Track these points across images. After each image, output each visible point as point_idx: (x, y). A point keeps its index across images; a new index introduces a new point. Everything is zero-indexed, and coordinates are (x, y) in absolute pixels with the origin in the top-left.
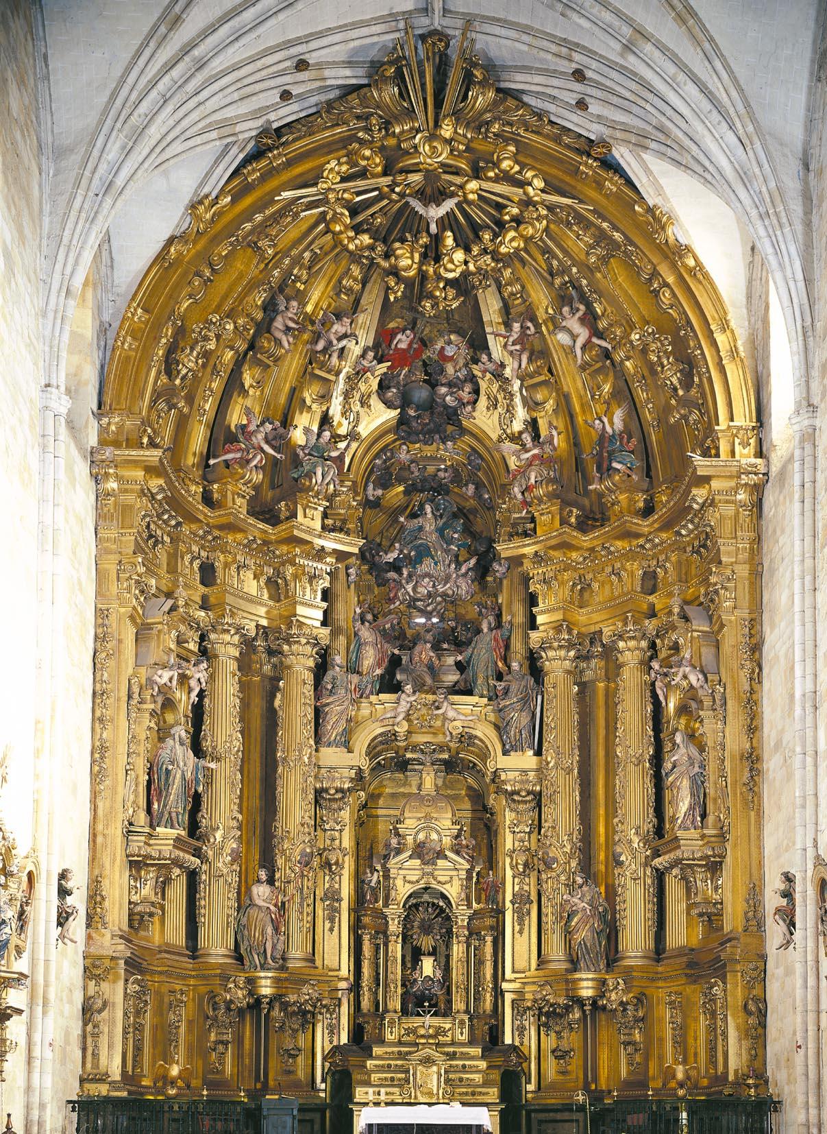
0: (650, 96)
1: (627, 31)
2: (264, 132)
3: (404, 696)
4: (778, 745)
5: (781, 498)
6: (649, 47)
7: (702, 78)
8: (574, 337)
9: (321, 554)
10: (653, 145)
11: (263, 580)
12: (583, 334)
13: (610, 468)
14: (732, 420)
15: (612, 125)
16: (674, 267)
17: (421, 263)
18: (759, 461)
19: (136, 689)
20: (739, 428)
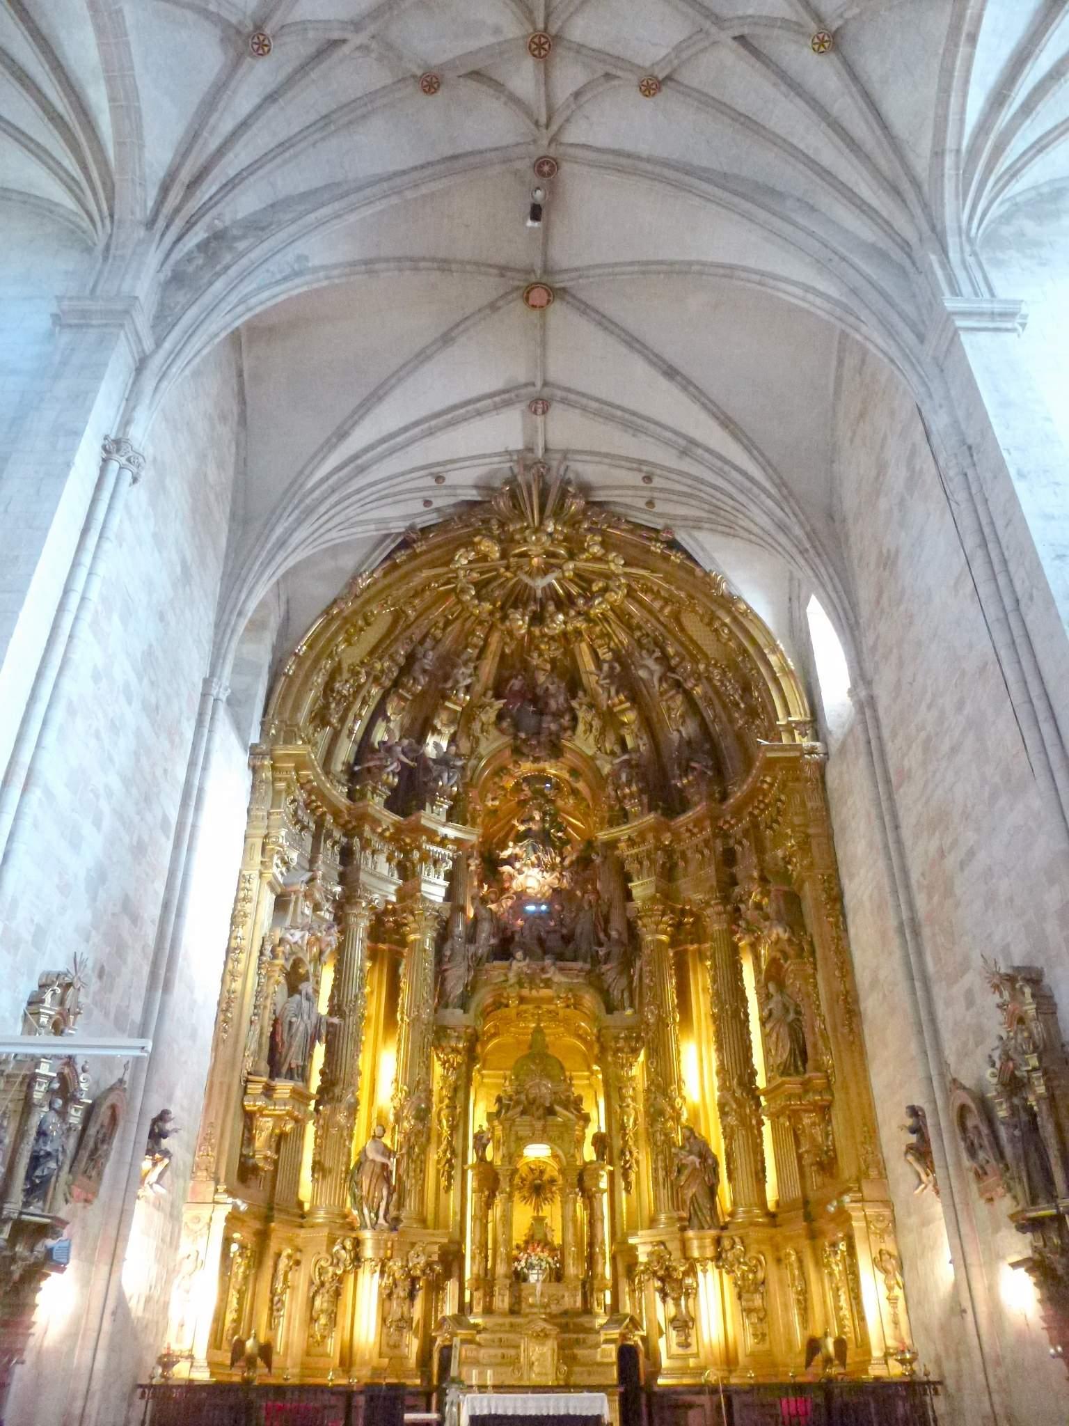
0: (703, 487)
1: (683, 442)
2: (411, 528)
4: (875, 982)
5: (845, 767)
6: (700, 451)
8: (651, 673)
9: (443, 842)
10: (707, 525)
11: (394, 863)
12: (656, 668)
13: (688, 766)
14: (789, 714)
15: (674, 517)
16: (729, 612)
17: (530, 625)
19: (268, 948)
20: (798, 723)
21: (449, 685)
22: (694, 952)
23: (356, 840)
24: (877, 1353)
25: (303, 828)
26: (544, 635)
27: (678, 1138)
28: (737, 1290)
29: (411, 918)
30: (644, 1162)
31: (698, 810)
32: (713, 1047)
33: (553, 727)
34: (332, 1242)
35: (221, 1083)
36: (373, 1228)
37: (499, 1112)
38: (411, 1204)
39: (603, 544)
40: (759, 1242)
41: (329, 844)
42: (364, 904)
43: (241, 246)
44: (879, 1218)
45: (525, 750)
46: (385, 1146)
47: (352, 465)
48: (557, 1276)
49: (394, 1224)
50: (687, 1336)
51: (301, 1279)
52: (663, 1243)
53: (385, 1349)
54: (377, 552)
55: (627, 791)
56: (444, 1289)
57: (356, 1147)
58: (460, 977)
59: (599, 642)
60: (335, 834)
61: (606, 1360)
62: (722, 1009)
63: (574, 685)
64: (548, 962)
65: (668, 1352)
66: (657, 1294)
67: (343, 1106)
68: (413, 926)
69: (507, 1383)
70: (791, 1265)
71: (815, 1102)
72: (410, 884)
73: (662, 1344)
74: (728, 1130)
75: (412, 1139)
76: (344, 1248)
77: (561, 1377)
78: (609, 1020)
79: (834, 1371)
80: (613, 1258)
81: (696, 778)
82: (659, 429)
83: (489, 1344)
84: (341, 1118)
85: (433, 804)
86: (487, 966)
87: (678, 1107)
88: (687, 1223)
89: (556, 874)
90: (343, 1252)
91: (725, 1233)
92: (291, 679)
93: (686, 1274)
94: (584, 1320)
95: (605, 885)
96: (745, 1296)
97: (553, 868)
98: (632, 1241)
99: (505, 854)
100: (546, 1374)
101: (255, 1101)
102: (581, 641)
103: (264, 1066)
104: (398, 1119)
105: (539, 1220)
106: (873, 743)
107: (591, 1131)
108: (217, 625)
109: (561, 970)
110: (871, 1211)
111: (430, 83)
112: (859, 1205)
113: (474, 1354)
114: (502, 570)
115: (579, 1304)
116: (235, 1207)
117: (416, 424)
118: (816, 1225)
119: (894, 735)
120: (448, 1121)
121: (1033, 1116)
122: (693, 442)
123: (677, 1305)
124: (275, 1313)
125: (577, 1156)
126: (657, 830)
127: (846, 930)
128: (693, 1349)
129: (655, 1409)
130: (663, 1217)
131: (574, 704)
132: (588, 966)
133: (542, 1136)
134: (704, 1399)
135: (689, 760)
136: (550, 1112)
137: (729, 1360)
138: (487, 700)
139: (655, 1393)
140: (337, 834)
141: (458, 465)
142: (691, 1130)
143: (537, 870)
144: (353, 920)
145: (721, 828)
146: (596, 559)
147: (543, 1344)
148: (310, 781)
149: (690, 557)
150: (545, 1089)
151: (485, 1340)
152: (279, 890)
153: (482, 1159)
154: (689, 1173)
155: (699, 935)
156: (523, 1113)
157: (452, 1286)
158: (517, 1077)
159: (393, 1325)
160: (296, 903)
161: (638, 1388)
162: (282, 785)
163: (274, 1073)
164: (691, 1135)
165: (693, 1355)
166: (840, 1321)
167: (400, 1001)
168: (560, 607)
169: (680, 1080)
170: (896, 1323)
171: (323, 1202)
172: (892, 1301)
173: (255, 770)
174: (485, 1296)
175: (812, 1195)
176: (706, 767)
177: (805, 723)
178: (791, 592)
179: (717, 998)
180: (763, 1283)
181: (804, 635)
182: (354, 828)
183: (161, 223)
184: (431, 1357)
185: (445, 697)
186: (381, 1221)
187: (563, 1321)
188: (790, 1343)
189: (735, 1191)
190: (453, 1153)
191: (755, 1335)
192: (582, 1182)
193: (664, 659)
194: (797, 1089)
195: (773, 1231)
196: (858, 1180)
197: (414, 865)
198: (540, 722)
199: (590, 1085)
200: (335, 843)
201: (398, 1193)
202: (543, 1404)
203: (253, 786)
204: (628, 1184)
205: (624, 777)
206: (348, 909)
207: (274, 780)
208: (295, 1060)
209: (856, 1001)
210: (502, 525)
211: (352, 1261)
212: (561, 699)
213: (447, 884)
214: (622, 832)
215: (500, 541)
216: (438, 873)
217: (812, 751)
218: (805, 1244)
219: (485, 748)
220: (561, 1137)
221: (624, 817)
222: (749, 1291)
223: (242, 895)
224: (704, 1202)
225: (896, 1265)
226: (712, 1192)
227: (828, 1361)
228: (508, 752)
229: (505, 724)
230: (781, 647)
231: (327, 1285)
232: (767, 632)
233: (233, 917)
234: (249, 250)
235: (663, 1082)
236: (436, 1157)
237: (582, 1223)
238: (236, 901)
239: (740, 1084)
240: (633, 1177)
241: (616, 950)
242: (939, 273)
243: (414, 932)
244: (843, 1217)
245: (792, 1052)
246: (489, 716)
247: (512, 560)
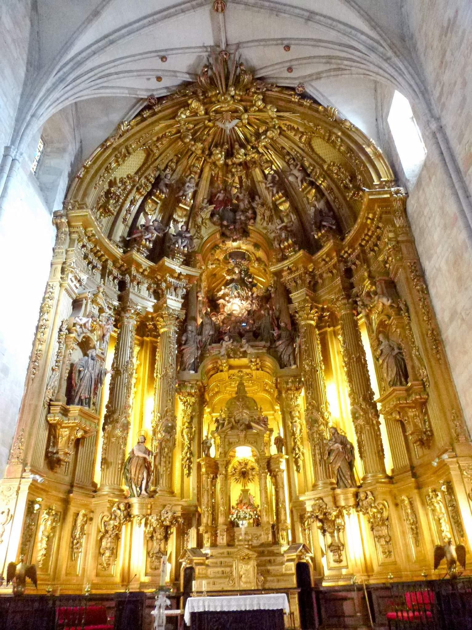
2: (152, 96)
3: (224, 343)
4: (454, 315)
11: (151, 291)
15: (305, 77)
16: (340, 129)
17: (225, 159)
19: (65, 326)
21: (181, 194)
22: (330, 332)
23: (127, 276)
25: (94, 267)
26: (233, 164)
27: (327, 435)
28: (370, 525)
29: (161, 319)
30: (306, 453)
31: (328, 246)
32: (345, 378)
33: (243, 218)
35: (30, 405)
38: (163, 482)
39: (264, 100)
40: (384, 493)
41: (111, 278)
42: (133, 311)
45: (228, 233)
46: (146, 449)
47: (107, 40)
48: (257, 523)
49: (152, 495)
51: (93, 529)
52: (321, 498)
53: (149, 570)
54: (132, 111)
55: (286, 244)
56: (187, 534)
57: (128, 450)
58: (191, 353)
59: (266, 165)
61: (288, 572)
62: (350, 359)
63: (253, 193)
65: (328, 566)
66: (319, 531)
67: (119, 425)
68: (163, 324)
69: (225, 589)
70: (405, 506)
71: (416, 399)
73: (323, 561)
74: (359, 428)
75: (163, 444)
76: (119, 509)
77: (260, 584)
79: (457, 569)
80: (292, 512)
81: (326, 231)
82: (292, 9)
83: (215, 565)
84: (118, 432)
87: (326, 417)
88: (336, 486)
89: (249, 302)
90: (118, 511)
91: (361, 490)
93: (337, 517)
94: (274, 548)
95: (278, 304)
96: (376, 528)
97: (247, 298)
98: (301, 499)
99: (221, 293)
100: (250, 582)
101: (54, 416)
102: (255, 167)
104: (154, 433)
105: (245, 492)
106: (445, 154)
107: (275, 435)
108: (17, 120)
109: (252, 346)
112: (455, 459)
113: (204, 572)
114: (206, 122)
115: (270, 538)
117: (145, 18)
118: (421, 479)
119: (461, 137)
120: (188, 435)
122: (312, 12)
124: (75, 550)
125: (266, 451)
127: (428, 293)
128: (344, 564)
129: (322, 602)
130: (320, 483)
131: (254, 205)
132: (268, 344)
133: (246, 441)
134: (354, 595)
135: (321, 221)
136: (249, 427)
137: (368, 570)
138: (204, 205)
139: (321, 592)
140: (115, 272)
141: (174, 52)
142: (335, 429)
143: (238, 299)
145: (342, 257)
146: (260, 110)
147: (247, 564)
148: (93, 235)
149: (316, 102)
150: (245, 415)
151: (213, 563)
152: (74, 297)
154: (335, 456)
155: (333, 320)
156: (232, 428)
158: (228, 409)
159: (156, 557)
160: (86, 305)
161: (312, 589)
163: (70, 400)
164: (335, 431)
165: (343, 567)
167: (156, 366)
168: (242, 146)
169: (326, 402)
171: (108, 482)
173: (58, 227)
174: (212, 535)
175: (416, 462)
176: (332, 224)
177: (391, 182)
178: (377, 116)
179: (348, 353)
180: (387, 519)
181: (386, 131)
182: (126, 270)
184: (179, 575)
185: (179, 201)
186: (143, 492)
187: (261, 549)
188: (408, 557)
191: (384, 553)
192: (269, 466)
193: (304, 169)
194: (404, 394)
195: (392, 486)
197: (163, 291)
198: (235, 216)
199: (275, 419)
200: (115, 278)
202: (242, 603)
203: (57, 236)
204: (298, 467)
205: (283, 235)
206: (123, 314)
208: (84, 393)
209: (439, 334)
210: (204, 93)
211: (125, 517)
212: (246, 202)
213: (183, 301)
215: (204, 104)
216: (177, 295)
218: (415, 493)
219: (205, 233)
220: (256, 442)
223: (47, 295)
224: (345, 470)
226: (351, 465)
227: (452, 562)
228: (218, 236)
229: (215, 219)
230: (373, 142)
231: (110, 532)
233: (42, 308)
235: (316, 405)
236: (181, 457)
237: (271, 495)
238: (44, 299)
239: (364, 399)
240: (300, 463)
241: (284, 334)
243: (163, 327)
246: (206, 214)
247: (211, 114)
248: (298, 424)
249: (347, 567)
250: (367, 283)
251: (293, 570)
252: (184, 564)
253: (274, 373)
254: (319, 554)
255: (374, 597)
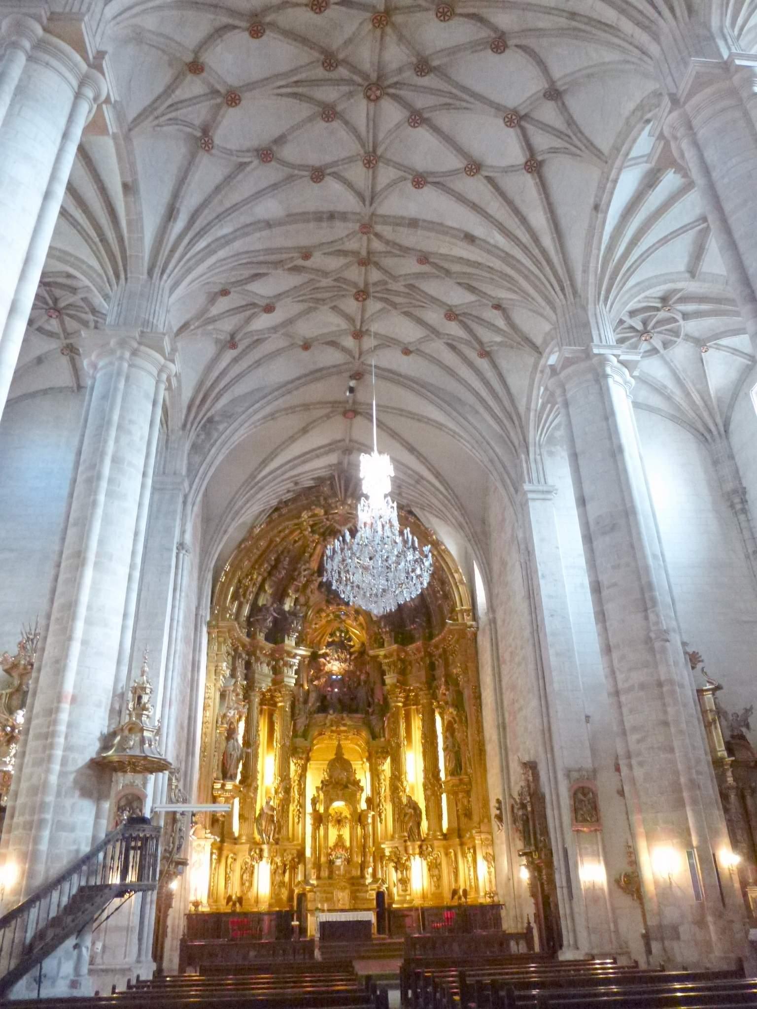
6: (425, 482)
7: (485, 725)
18: (474, 623)
21: (296, 573)
24: (482, 894)
27: (405, 800)
30: (388, 809)
31: (419, 643)
32: (421, 755)
34: (250, 850)
36: (268, 843)
37: (322, 788)
43: (221, 427)
44: (487, 839)
50: (406, 887)
60: (244, 660)
64: (345, 715)
72: (279, 677)
73: (395, 890)
78: (374, 743)
85: (288, 636)
86: (316, 715)
92: (223, 584)
93: (406, 860)
94: (361, 881)
97: (345, 661)
98: (383, 846)
103: (221, 776)
104: (276, 792)
105: (340, 837)
110: (483, 836)
111: (306, 347)
116: (215, 840)
121: (528, 818)
123: (402, 873)
126: (398, 652)
128: (408, 892)
134: (413, 913)
137: (424, 897)
140: (244, 656)
142: (410, 797)
144: (252, 698)
153: (315, 810)
154: (408, 814)
157: (300, 867)
159: (277, 885)
162: (221, 639)
166: (470, 880)
170: (490, 882)
172: (490, 873)
183: (188, 426)
189: (429, 824)
190: (300, 806)
192: (359, 819)
196: (479, 824)
201: (279, 829)
207: (218, 637)
208: (231, 771)
209: (484, 745)
210: (325, 499)
214: (382, 652)
215: (324, 507)
217: (471, 626)
221: (382, 645)
222: (434, 867)
225: (491, 859)
229: (323, 590)
232: (453, 560)
234: (226, 429)
239: (433, 776)
240: (383, 816)
242: (524, 465)
244: (472, 838)
245: (456, 765)
248: (383, 786)
249: (410, 895)
250: (443, 687)
251: (374, 896)
252: (296, 891)
253: (368, 743)
254: (392, 885)
255: (426, 914)
